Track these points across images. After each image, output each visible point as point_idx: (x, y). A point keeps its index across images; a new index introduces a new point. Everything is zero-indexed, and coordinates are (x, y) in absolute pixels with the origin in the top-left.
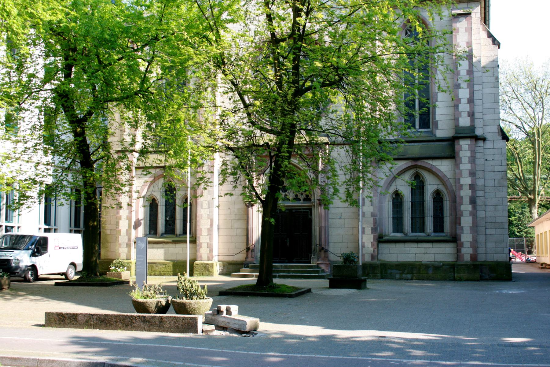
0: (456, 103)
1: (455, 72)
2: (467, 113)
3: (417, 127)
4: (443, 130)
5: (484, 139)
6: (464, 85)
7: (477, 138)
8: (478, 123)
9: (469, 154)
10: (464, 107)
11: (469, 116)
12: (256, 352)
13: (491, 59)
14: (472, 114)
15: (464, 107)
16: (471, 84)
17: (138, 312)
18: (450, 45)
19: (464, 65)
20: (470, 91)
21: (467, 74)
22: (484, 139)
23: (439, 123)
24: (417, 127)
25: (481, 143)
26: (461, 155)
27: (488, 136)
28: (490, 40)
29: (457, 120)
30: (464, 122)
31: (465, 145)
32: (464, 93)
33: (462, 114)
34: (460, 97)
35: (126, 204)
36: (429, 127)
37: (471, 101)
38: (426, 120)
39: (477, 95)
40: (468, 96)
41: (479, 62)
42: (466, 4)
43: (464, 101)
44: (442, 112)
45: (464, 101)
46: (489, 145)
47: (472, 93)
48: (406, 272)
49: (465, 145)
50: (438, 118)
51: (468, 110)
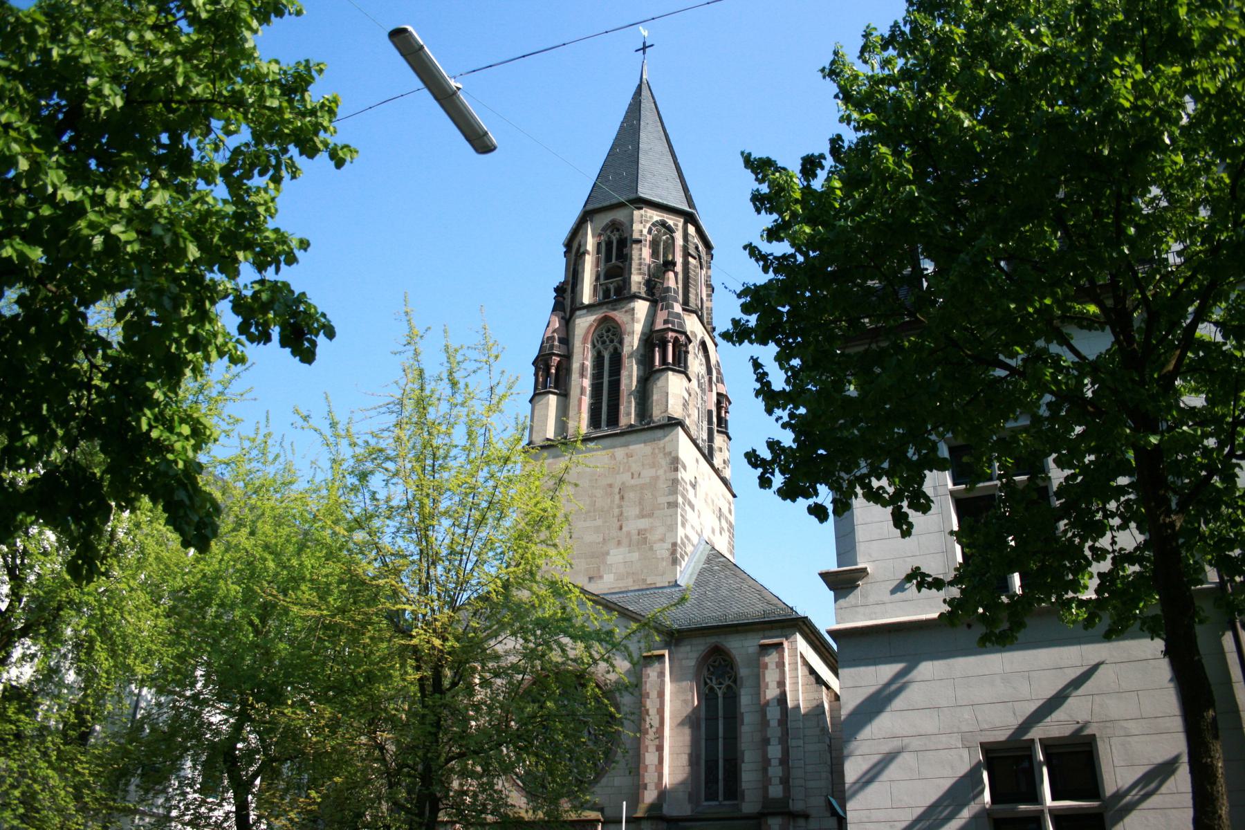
0: (766, 762)
1: (764, 723)
3: (721, 798)
4: (750, 805)
5: (806, 817)
6: (774, 741)
7: (794, 816)
9: (771, 771)
10: (775, 771)
13: (815, 703)
14: (785, 781)
16: (784, 740)
17: (982, 791)
18: (758, 684)
19: (774, 714)
22: (806, 817)
24: (721, 798)
25: (801, 822)
28: (812, 679)
29: (765, 789)
30: (776, 791)
32: (774, 751)
37: (784, 761)
38: (733, 790)
41: (798, 707)
43: (775, 762)
44: (748, 777)
45: (775, 762)
46: (813, 824)
47: (786, 752)
48: (967, 550)
50: (744, 786)
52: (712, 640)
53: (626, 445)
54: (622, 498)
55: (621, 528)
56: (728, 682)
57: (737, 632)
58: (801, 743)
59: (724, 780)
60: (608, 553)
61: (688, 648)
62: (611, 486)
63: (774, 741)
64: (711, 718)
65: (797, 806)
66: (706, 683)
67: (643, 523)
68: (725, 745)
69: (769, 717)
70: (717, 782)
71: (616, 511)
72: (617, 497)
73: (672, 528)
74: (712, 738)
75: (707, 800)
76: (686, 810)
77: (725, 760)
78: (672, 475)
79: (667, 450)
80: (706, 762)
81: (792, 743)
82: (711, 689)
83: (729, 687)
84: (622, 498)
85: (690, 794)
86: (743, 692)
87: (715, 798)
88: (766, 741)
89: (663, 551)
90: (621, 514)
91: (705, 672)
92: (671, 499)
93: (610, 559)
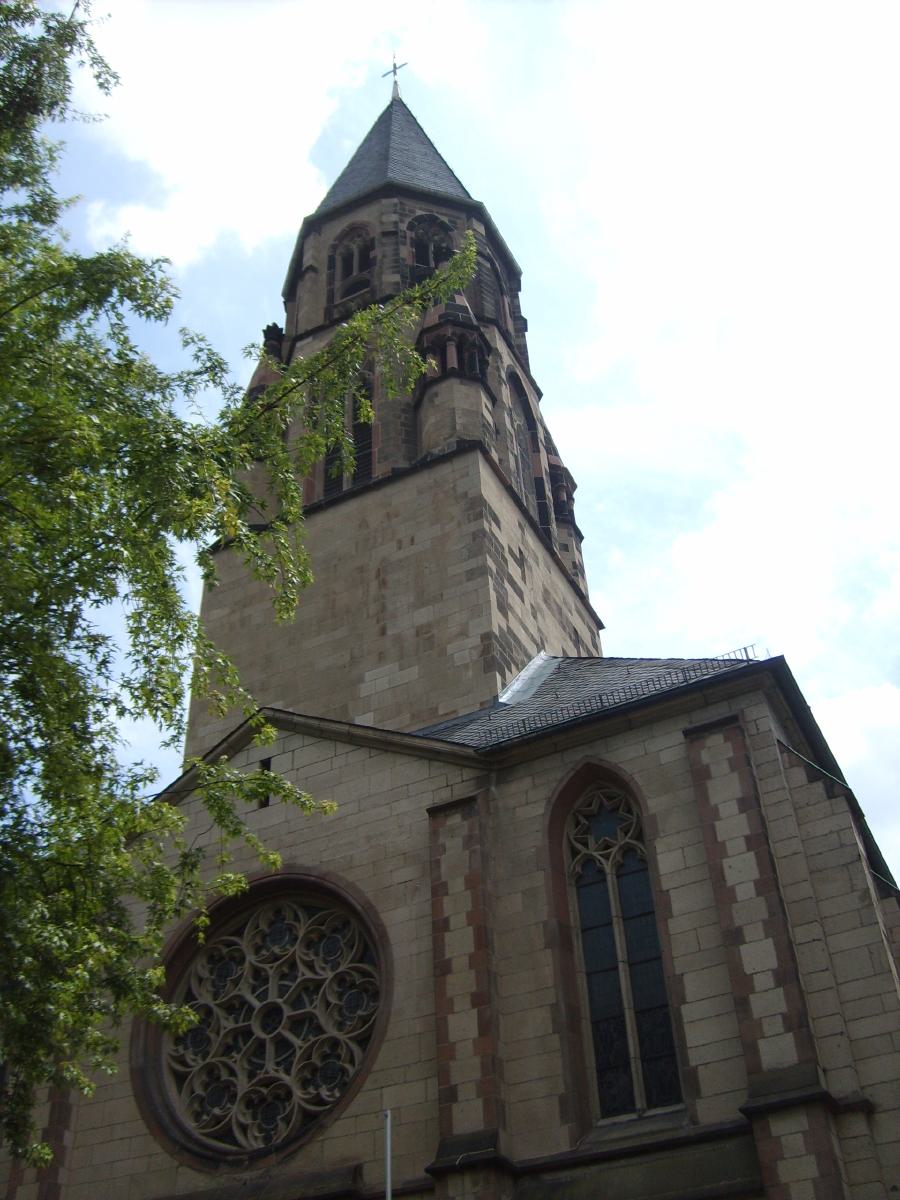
0: (740, 988)
2: (779, 1019)
3: (640, 1103)
4: (716, 1102)
6: (754, 932)
7: (833, 1108)
8: (832, 1053)
9: (723, 829)
10: (768, 1002)
11: (788, 1029)
12: (392, 1150)
14: (798, 1022)
15: (768, 1002)
16: (778, 924)
20: (777, 944)
21: (759, 894)
23: (702, 1073)
24: (640, 1102)
25: (857, 1125)
26: (784, 1178)
27: (883, 1097)
29: (750, 1050)
30: (778, 1051)
31: (790, 1132)
32: (759, 955)
33: (766, 1027)
34: (748, 970)
35: (231, 367)
36: (679, 1100)
37: (787, 974)
38: (669, 1078)
39: (809, 959)
40: (772, 962)
42: (725, 703)
43: (764, 981)
44: (703, 1033)
45: (764, 981)
47: (787, 952)
49: (790, 1132)
50: (694, 1058)
51: (783, 1007)
52: (577, 757)
53: (561, 1154)
54: (383, 584)
55: (383, 632)
56: (623, 840)
57: (630, 727)
58: (816, 930)
59: (645, 1059)
60: (361, 680)
61: (527, 783)
62: (361, 569)
63: (754, 932)
64: (596, 927)
65: (840, 1085)
66: (574, 852)
67: (423, 616)
68: (633, 977)
69: (731, 877)
70: (627, 1065)
71: (373, 609)
72: (374, 585)
73: (480, 610)
74: (602, 971)
76: (557, 1141)
77: (639, 1013)
78: (472, 527)
79: (460, 490)
80: (595, 1024)
81: (800, 934)
82: (589, 861)
83: (628, 851)
84: (383, 584)
85: (563, 1101)
86: (660, 845)
87: (628, 1106)
88: (734, 937)
89: (464, 651)
90: (383, 608)
91: (570, 830)
92: (473, 564)
93: (365, 690)
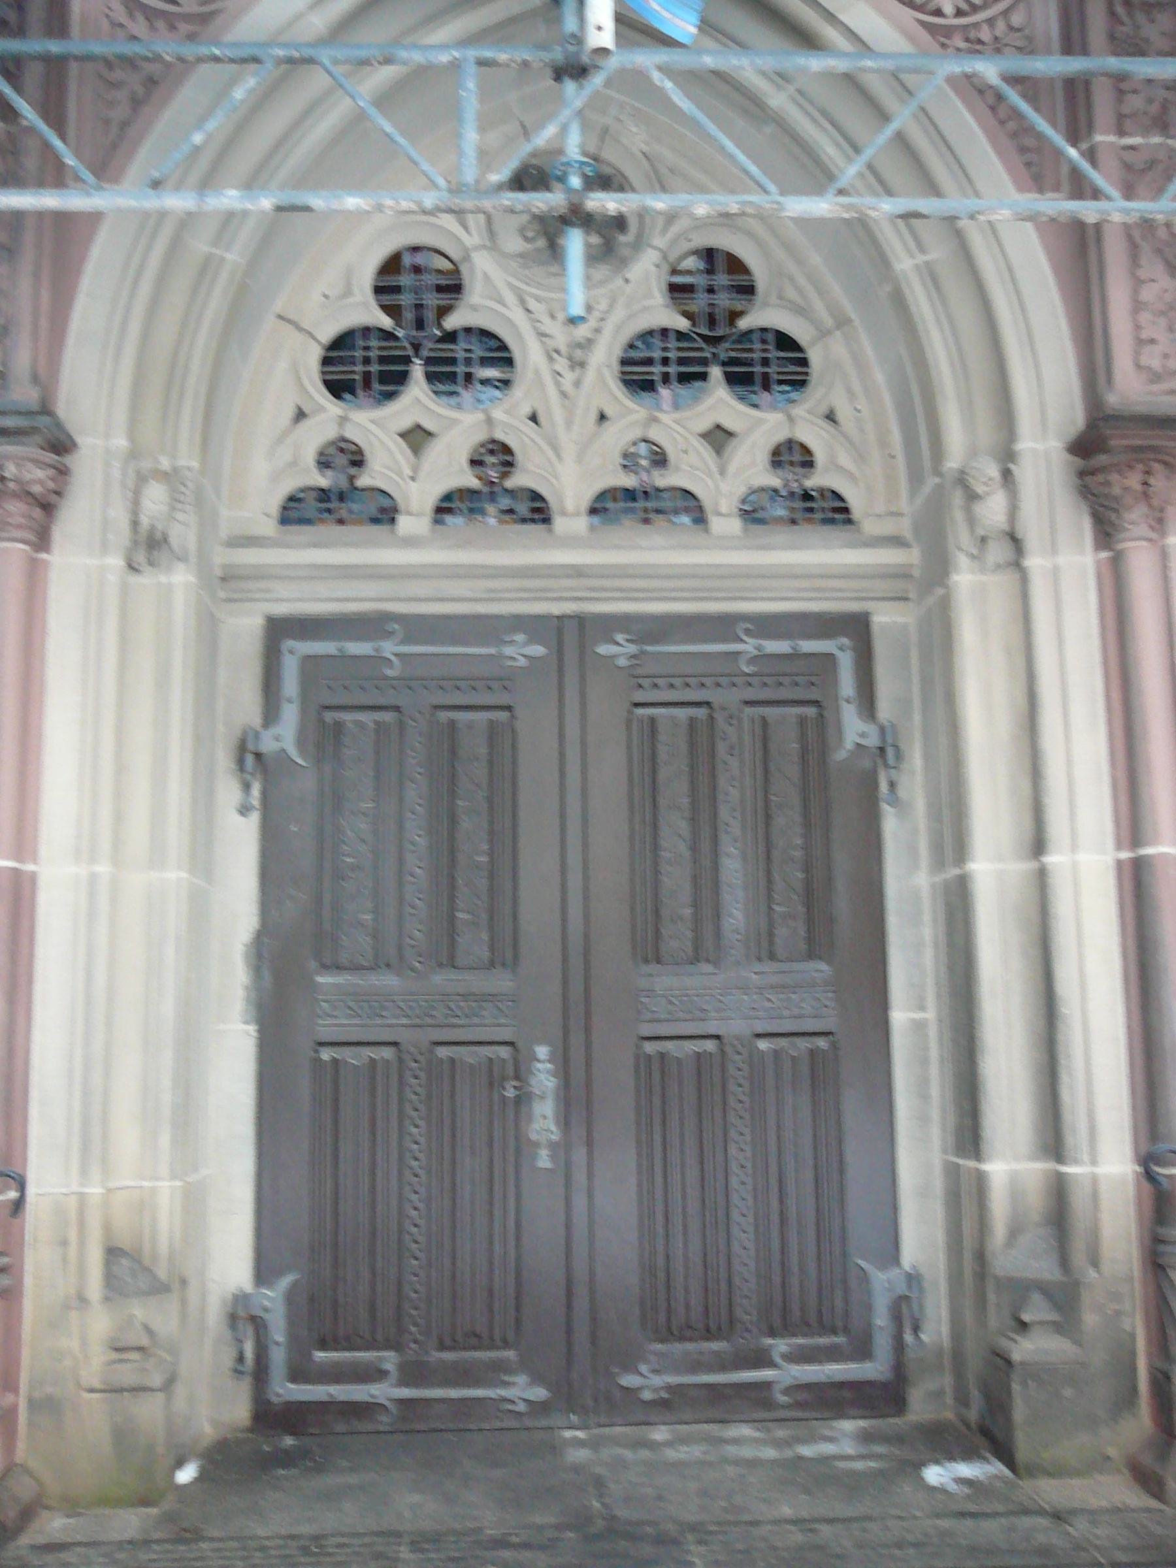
75: (829, 659)
